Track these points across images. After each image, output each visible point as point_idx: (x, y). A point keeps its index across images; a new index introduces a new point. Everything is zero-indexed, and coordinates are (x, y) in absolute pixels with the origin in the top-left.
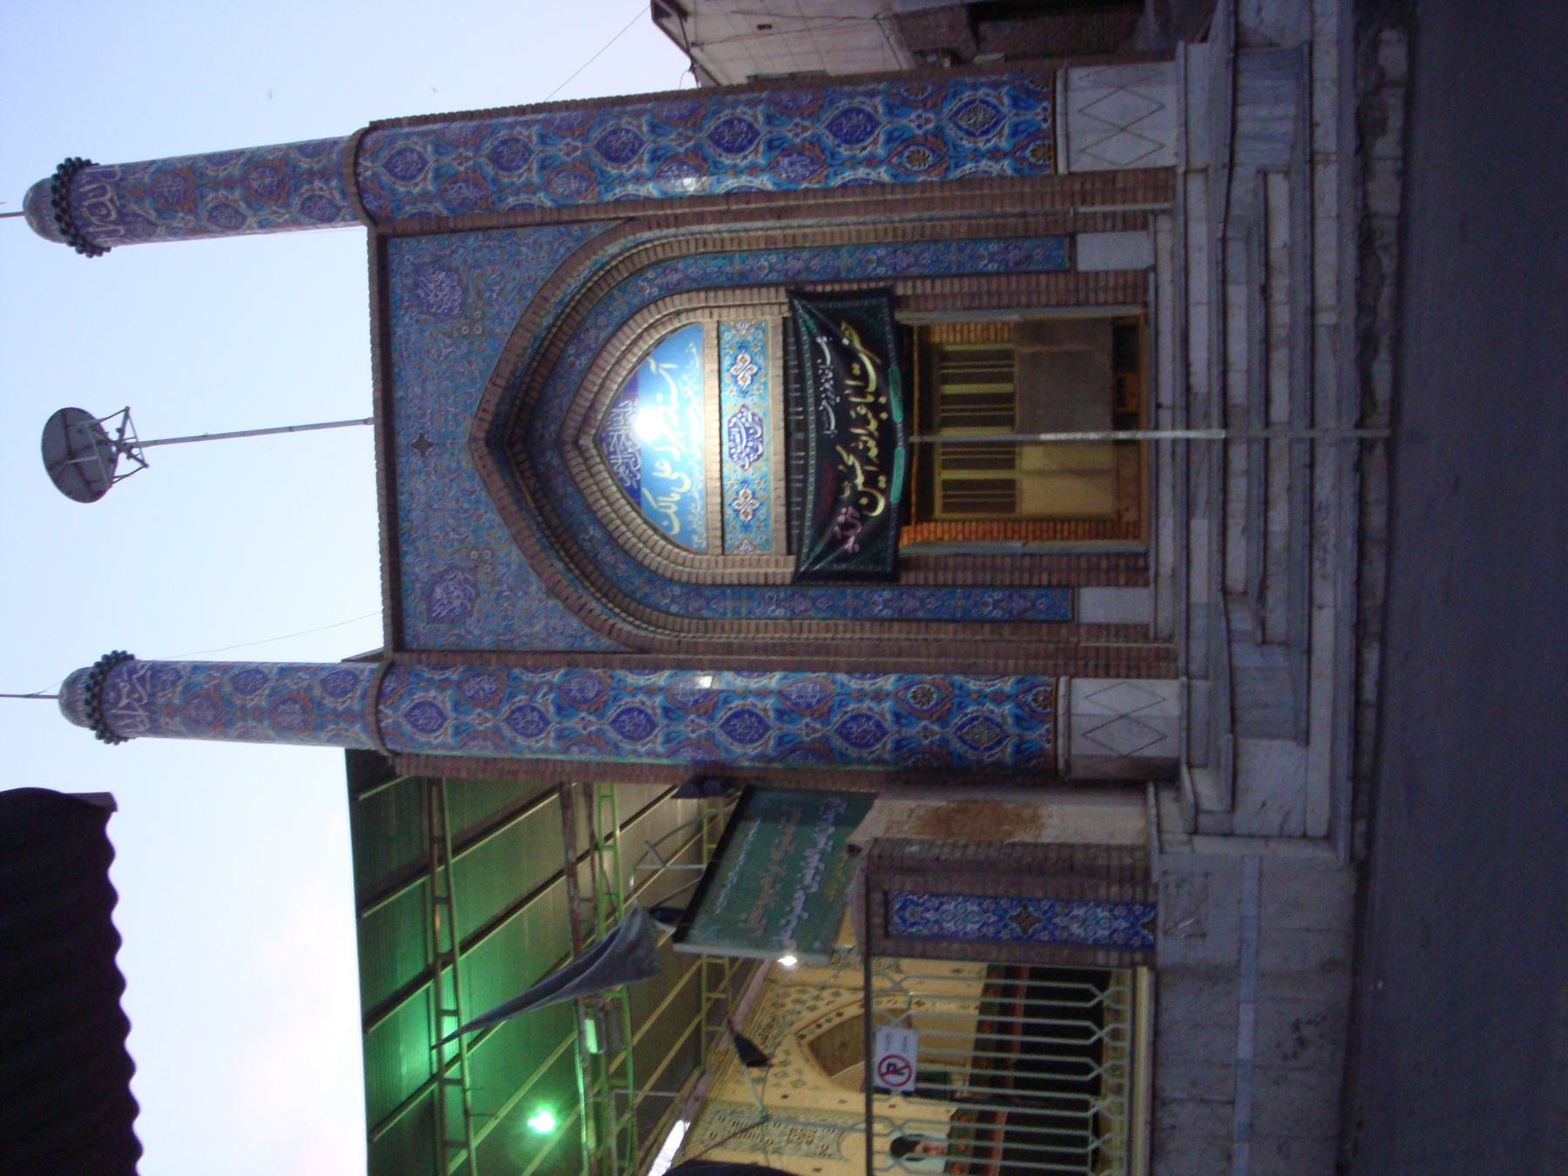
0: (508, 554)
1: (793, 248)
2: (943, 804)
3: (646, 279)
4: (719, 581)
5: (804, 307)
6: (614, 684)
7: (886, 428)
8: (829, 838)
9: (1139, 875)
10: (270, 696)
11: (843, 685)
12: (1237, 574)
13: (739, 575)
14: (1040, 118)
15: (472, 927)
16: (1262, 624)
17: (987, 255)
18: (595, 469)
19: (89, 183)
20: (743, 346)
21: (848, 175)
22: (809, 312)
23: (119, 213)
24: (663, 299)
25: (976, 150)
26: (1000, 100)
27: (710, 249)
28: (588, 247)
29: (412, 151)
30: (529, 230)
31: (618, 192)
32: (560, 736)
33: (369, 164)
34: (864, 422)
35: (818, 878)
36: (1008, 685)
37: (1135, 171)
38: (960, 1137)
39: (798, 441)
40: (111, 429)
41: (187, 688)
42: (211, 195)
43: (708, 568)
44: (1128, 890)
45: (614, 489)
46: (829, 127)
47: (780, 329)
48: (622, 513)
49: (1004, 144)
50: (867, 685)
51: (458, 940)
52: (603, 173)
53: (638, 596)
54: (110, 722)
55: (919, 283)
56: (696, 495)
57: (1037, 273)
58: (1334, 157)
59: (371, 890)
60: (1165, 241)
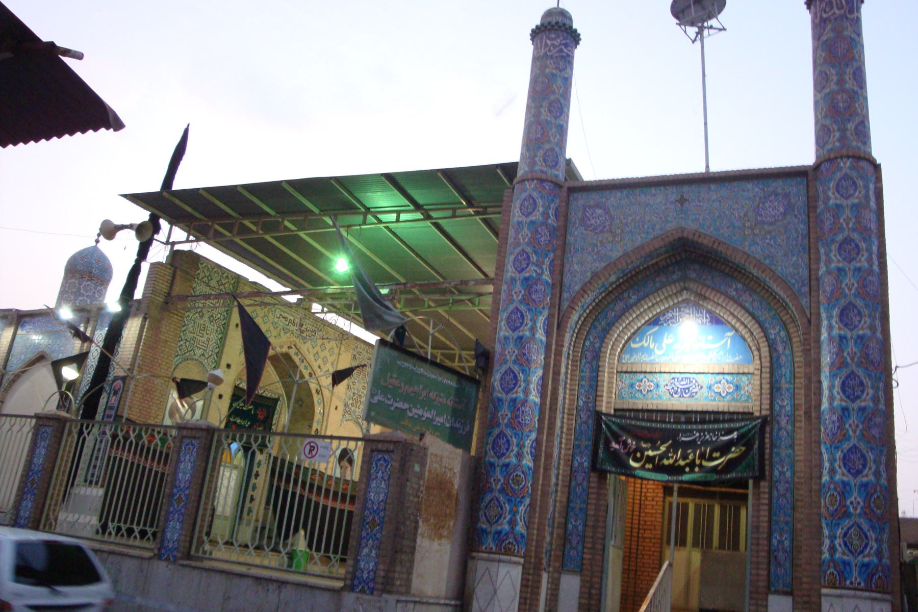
3: (780, 331)
4: (600, 369)
5: (756, 425)
7: (679, 470)
8: (443, 424)
11: (528, 436)
14: (853, 580)
17: (781, 539)
18: (669, 299)
20: (737, 388)
21: (826, 456)
22: (753, 428)
25: (835, 538)
26: (869, 555)
28: (795, 296)
29: (855, 190)
30: (807, 261)
31: (824, 315)
34: (684, 457)
36: (520, 528)
38: (336, 483)
39: (680, 418)
40: (713, 22)
41: (553, 75)
42: (833, 71)
44: (380, 580)
45: (658, 310)
47: (746, 410)
49: (838, 555)
50: (527, 449)
51: (440, 221)
52: (834, 306)
54: (540, 36)
56: (652, 358)
59: (452, 176)
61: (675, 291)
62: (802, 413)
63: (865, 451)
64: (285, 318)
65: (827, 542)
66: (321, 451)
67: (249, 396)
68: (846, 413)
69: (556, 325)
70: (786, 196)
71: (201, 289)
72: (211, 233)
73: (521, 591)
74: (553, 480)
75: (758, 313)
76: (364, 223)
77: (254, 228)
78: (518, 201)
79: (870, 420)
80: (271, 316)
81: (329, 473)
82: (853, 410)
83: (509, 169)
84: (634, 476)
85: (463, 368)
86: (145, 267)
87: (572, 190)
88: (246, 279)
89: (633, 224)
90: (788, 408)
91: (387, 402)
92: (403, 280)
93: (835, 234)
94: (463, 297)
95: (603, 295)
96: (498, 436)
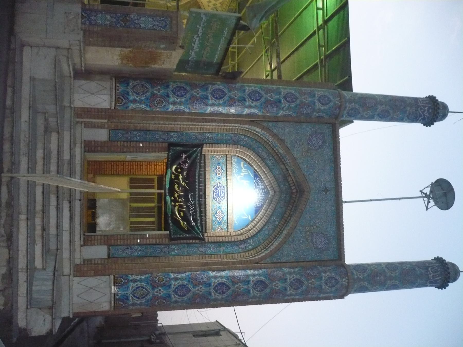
1: (203, 254)
2: (153, 66)
4: (228, 145)
6: (262, 109)
10: (377, 109)
11: (186, 108)
12: (54, 137)
15: (312, 39)
16: (46, 120)
19: (438, 280)
20: (220, 223)
21: (184, 275)
22: (198, 233)
23: (428, 270)
24: (246, 239)
25: (141, 282)
27: (230, 255)
28: (271, 255)
29: (329, 287)
30: (291, 261)
31: (260, 272)
32: (280, 93)
33: (344, 283)
36: (131, 106)
37: (87, 276)
39: (201, 192)
40: (432, 203)
41: (405, 112)
42: (397, 274)
43: (231, 150)
46: (190, 290)
47: (207, 228)
49: (131, 284)
50: (178, 107)
51: (317, 36)
56: (235, 174)
58: (20, 270)
59: (344, 48)
60: (77, 255)
61: (274, 186)
63: (188, 295)
65: (138, 278)
68: (207, 286)
69: (253, 120)
78: (326, 95)
79: (204, 298)
82: (210, 289)
84: (167, 169)
89: (313, 162)
90: (209, 251)
91: (202, 23)
93: (305, 277)
95: (271, 145)
96: (185, 89)
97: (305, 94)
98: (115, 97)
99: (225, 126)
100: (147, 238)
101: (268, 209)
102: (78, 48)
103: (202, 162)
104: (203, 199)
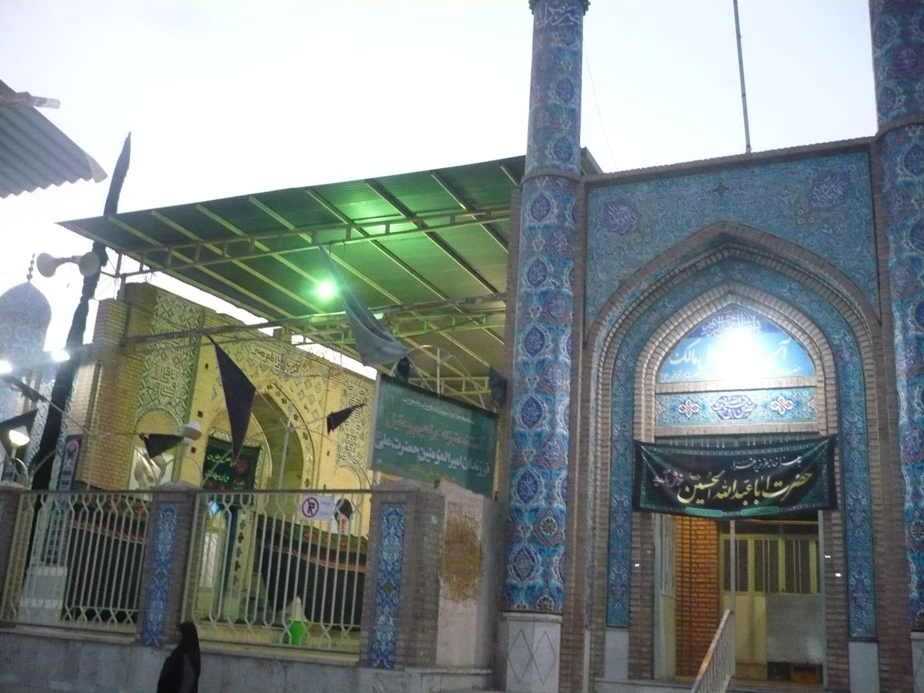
0: (647, 253)
6: (560, 328)
7: (738, 505)
8: (459, 467)
9: (411, 660)
10: (556, 105)
11: (558, 475)
13: (640, 405)
18: (712, 306)
20: (798, 404)
21: (908, 479)
24: (830, 347)
28: (860, 292)
30: (873, 251)
31: (897, 314)
33: (918, 133)
35: (428, 461)
36: (555, 582)
41: (559, 49)
42: (895, 22)
43: (645, 383)
44: (400, 652)
45: (700, 319)
47: (810, 430)
48: (683, 326)
50: (558, 490)
51: (437, 231)
52: (909, 303)
53: (627, 339)
55: (840, 528)
56: (695, 375)
57: (848, 614)
59: (450, 178)
61: (718, 296)
62: (876, 429)
64: (262, 353)
66: (322, 508)
67: (236, 451)
69: (583, 345)
70: (845, 176)
71: (162, 326)
72: (169, 261)
73: (561, 654)
74: (590, 523)
75: (818, 316)
76: (349, 238)
77: (219, 252)
78: (540, 203)
80: (244, 352)
81: (325, 529)
83: (515, 165)
85: (475, 397)
86: (93, 306)
87: (590, 186)
88: (213, 312)
89: (664, 221)
90: (860, 425)
91: (394, 446)
92: (398, 303)
93: (906, 218)
94: (470, 318)
95: (634, 305)
96: (524, 477)
97: (529, 247)
98: (536, 612)
99: (597, 399)
100: (833, 558)
101: (765, 306)
102: (437, 679)
103: (671, 442)
104: (748, 440)
